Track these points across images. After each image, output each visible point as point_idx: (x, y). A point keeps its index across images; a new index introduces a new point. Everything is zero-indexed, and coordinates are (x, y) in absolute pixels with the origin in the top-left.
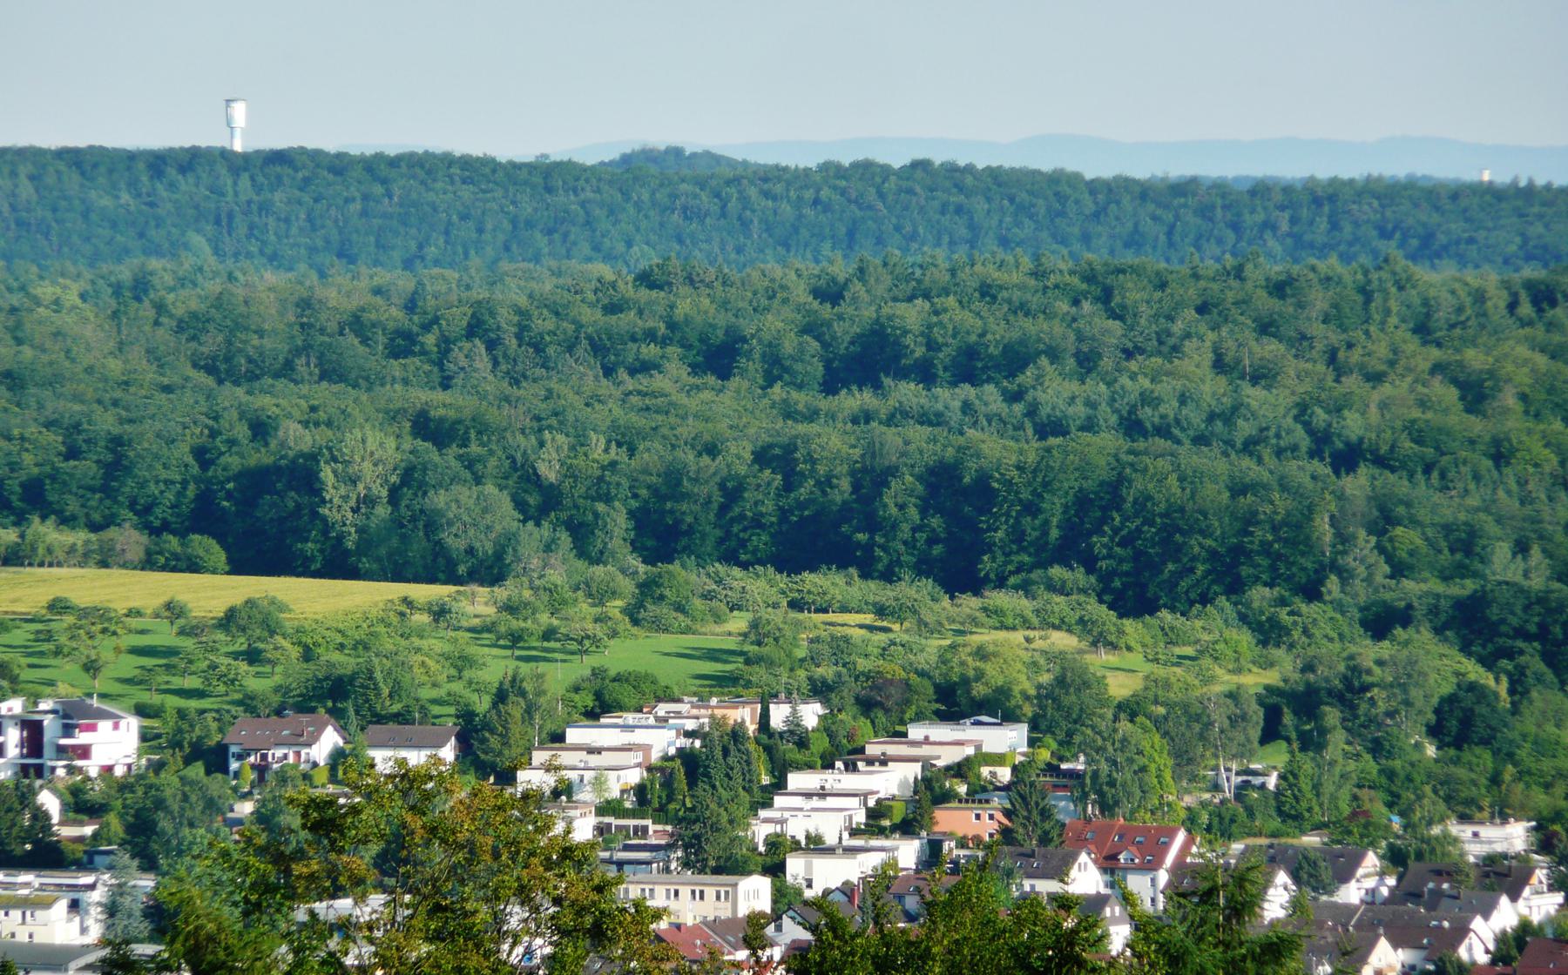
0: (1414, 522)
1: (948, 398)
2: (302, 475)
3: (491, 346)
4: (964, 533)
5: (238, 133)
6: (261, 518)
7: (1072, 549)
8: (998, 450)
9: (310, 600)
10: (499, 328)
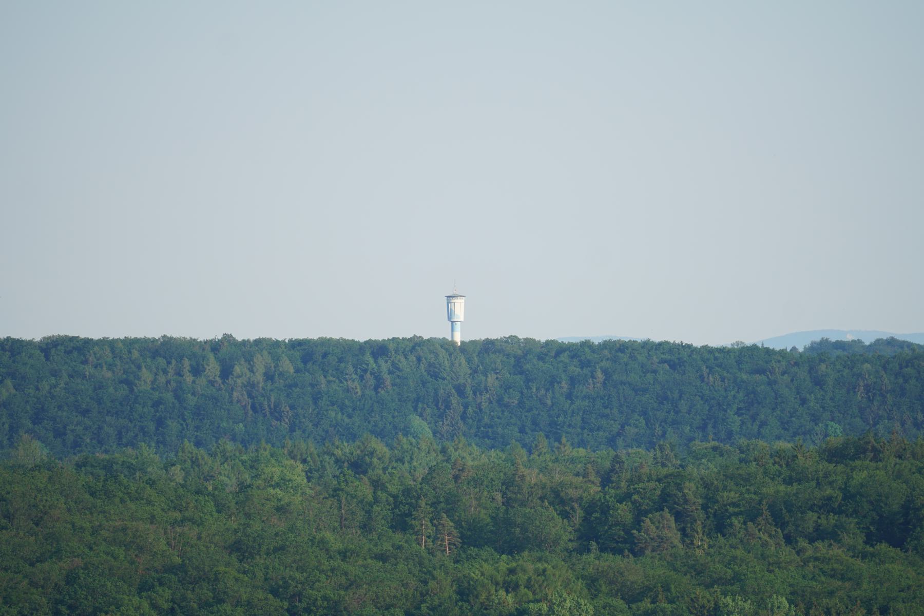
0: (690, 480)
3: (678, 516)
5: (458, 326)
10: (686, 501)
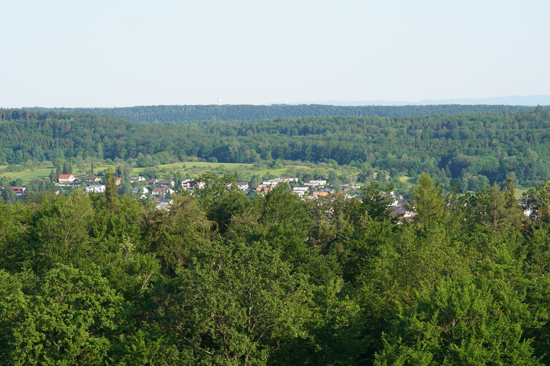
1: (315, 136)
2: (226, 148)
4: (317, 156)
6: (222, 154)
7: (332, 157)
8: (321, 144)
9: (228, 166)
